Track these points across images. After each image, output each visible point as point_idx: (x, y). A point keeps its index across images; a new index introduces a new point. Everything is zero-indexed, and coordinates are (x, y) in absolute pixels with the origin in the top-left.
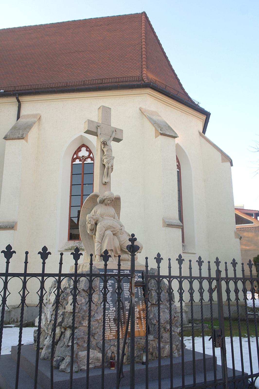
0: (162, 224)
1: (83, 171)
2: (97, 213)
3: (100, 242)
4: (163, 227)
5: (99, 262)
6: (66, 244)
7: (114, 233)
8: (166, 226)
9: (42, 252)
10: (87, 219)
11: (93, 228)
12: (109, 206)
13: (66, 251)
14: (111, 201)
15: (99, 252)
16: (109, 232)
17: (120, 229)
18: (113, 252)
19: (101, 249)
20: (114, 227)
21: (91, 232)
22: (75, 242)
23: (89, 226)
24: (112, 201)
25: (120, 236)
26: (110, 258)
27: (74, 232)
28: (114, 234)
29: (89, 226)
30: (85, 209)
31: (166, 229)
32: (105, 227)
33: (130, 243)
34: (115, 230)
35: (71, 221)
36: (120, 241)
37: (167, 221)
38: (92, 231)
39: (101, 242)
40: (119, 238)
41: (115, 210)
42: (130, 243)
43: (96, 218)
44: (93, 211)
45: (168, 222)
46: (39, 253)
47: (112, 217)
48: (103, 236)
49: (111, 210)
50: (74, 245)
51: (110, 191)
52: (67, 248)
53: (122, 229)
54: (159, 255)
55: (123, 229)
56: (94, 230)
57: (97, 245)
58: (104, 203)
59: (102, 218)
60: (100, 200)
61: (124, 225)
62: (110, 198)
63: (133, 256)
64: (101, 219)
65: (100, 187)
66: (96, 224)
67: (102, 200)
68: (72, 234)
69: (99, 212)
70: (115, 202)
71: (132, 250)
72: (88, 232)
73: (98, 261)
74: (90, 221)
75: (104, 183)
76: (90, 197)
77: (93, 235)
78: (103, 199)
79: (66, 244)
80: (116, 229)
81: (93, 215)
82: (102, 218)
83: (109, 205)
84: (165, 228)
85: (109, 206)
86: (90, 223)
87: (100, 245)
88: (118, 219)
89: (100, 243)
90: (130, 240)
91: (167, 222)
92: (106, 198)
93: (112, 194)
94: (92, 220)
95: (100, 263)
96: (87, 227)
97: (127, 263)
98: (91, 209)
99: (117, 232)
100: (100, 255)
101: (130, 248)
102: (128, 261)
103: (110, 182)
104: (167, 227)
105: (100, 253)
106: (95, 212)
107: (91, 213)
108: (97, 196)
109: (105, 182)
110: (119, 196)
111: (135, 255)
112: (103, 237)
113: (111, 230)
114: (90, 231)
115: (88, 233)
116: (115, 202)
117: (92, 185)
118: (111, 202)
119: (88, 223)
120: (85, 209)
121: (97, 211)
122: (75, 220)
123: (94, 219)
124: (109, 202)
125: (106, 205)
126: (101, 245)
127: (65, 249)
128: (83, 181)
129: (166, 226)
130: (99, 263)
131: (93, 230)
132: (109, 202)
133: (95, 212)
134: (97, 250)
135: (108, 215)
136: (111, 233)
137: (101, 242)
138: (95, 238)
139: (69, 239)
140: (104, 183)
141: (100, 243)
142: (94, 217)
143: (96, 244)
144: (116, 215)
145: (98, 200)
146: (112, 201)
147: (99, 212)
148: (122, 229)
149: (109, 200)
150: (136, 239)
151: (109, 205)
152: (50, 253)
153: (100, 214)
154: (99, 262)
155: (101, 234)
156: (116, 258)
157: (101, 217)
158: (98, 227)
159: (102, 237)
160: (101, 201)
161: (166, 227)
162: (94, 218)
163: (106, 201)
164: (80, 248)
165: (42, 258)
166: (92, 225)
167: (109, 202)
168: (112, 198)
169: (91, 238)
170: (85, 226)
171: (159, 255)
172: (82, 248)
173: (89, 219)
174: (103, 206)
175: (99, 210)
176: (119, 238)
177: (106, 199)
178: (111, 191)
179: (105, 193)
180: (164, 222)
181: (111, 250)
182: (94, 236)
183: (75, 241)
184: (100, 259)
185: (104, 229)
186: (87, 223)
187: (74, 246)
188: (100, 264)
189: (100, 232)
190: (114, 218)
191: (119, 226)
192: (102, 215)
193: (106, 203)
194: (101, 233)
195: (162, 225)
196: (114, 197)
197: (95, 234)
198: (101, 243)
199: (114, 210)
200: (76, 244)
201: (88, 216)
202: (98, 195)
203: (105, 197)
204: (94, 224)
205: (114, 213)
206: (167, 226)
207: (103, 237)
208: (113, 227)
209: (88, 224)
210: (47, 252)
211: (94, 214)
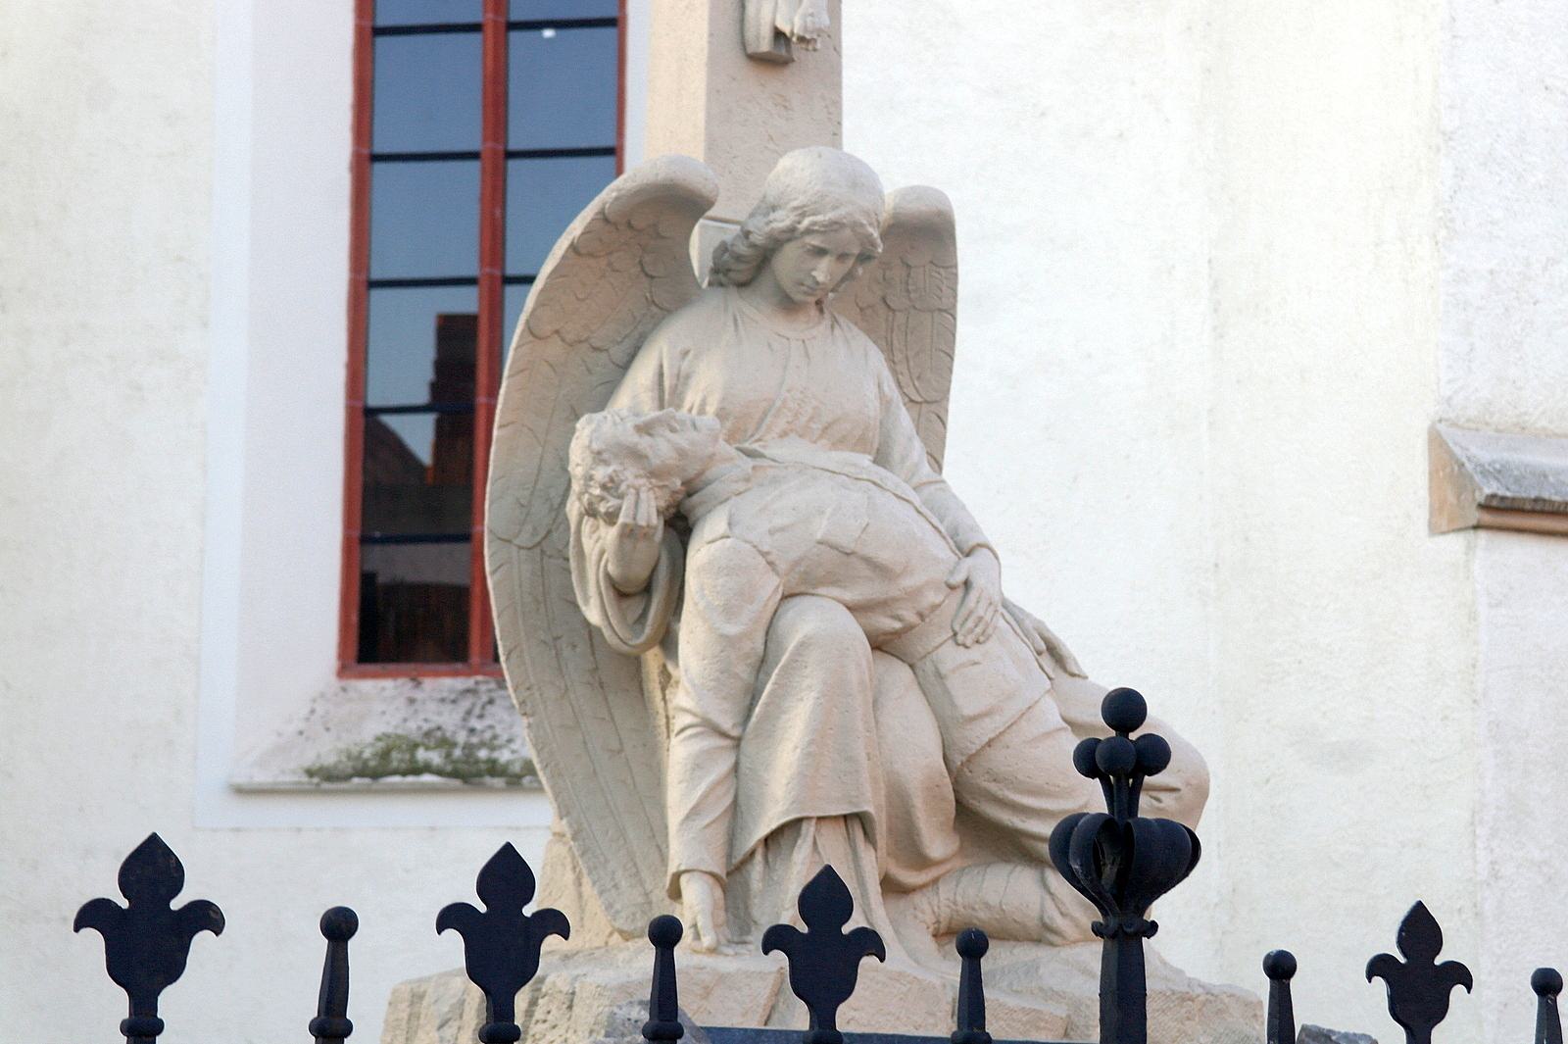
0: (1423, 493)
1: (495, 196)
2: (692, 398)
3: (727, 723)
4: (1434, 530)
5: (713, 951)
6: (320, 710)
7: (890, 624)
8: (1475, 516)
9: (124, 904)
10: (569, 460)
11: (641, 573)
12: (827, 321)
13: (316, 791)
14: (842, 257)
15: (719, 835)
16: (822, 623)
17: (952, 588)
18: (869, 836)
19: (735, 803)
20: (884, 556)
21: (623, 618)
22: (419, 695)
23: (598, 544)
24: (864, 258)
25: (950, 657)
26: (868, 962)
27: (417, 564)
28: (880, 644)
29: (598, 544)
30: (554, 349)
31: (1470, 549)
32: (782, 566)
33: (1091, 798)
34: (893, 591)
35: (369, 434)
36: (947, 724)
37: (1485, 456)
38: (635, 607)
39: (738, 735)
40: (933, 688)
41: (891, 361)
42: (1091, 798)
43: (682, 453)
44: (642, 374)
45: (1498, 473)
46: (93, 914)
47: (860, 444)
48: (763, 664)
49: (849, 366)
50: (413, 727)
51: (835, 137)
52: (326, 751)
53: (967, 584)
54: (1420, 929)
55: (979, 582)
56: (652, 589)
57: (698, 765)
58: (765, 283)
59: (750, 454)
60: (723, 248)
61: (990, 533)
62: (835, 226)
63: (1125, 936)
64: (731, 467)
65: (714, 92)
66: (680, 524)
67: (742, 249)
68: (381, 579)
69: (707, 386)
70: (895, 273)
71: (1109, 871)
72: (593, 614)
73: (707, 940)
74: (610, 487)
75: (765, 45)
76: (603, 217)
77: (647, 645)
78: (757, 238)
79: (320, 710)
80: (908, 582)
81: (645, 429)
82: (750, 454)
83: (819, 303)
84: (1455, 543)
85: (827, 321)
86: (611, 518)
87: (730, 761)
88: (926, 470)
89: (724, 735)
90: (1088, 760)
91: (1485, 473)
92: (792, 230)
93: (860, 179)
94: (630, 475)
95: (726, 964)
96: (571, 552)
97: (1032, 969)
98: (618, 353)
99: (911, 617)
100: (720, 871)
101: (1094, 863)
102: (1038, 941)
103: (831, 35)
104: (1483, 535)
105: (729, 856)
106: (668, 393)
107: (622, 400)
108: (677, 204)
109: (779, 35)
110: (942, 197)
111: (1152, 928)
112: (755, 675)
113: (849, 596)
114: (609, 597)
115: (587, 624)
116: (895, 273)
117: (609, 33)
118: (849, 276)
119: (591, 512)
120: (554, 349)
121: (683, 380)
122: (419, 436)
123: (653, 474)
124: (823, 271)
125: (788, 305)
126: (736, 768)
127: (310, 773)
128: (495, 196)
129: (1475, 516)
130: (709, 961)
131: (647, 589)
132: (821, 275)
133: (668, 393)
134: (688, 817)
135: (816, 426)
136: (852, 630)
137: (738, 735)
138: (666, 678)
139: (353, 650)
140: (765, 45)
141: (724, 735)
142: (661, 448)
143: (679, 753)
144: (904, 419)
145: (700, 245)
146: (864, 258)
147: (707, 386)
148: (967, 584)
149: (821, 252)
150: (1155, 755)
151: (819, 303)
152: (205, 916)
153: (722, 415)
154: (713, 951)
155: (729, 642)
156: (902, 903)
157: (731, 450)
158: (699, 554)
159: (744, 672)
160: (738, 258)
161: (1476, 527)
162: (656, 462)
163: (786, 263)
164: (483, 754)
165: (118, 970)
166: (630, 533)
167: (823, 271)
168: (856, 226)
169: (625, 675)
170: (551, 549)
171: (1420, 929)
172: (504, 756)
173: (601, 473)
174: (756, 316)
175: (706, 366)
176: (933, 688)
177: (791, 234)
178: (847, 148)
179: (785, 162)
180: (1449, 468)
181: (845, 817)
182: (653, 659)
183: (416, 681)
184: (722, 916)
185: (770, 587)
186: (573, 508)
187: (417, 737)
188: (722, 978)
189: (729, 611)
190: (881, 458)
191: (943, 551)
192: (741, 427)
193: (787, 284)
194: (732, 629)
195: (1422, 516)
196: (884, 216)
197: (667, 641)
198: (737, 742)
199: (877, 359)
200: (432, 706)
201: (586, 433)
202: (706, 189)
203: (782, 220)
204: (656, 521)
205: (886, 403)
206: (1487, 518)
207: (755, 675)
208: (868, 561)
209: (588, 524)
210: (176, 904)
211: (650, 412)
